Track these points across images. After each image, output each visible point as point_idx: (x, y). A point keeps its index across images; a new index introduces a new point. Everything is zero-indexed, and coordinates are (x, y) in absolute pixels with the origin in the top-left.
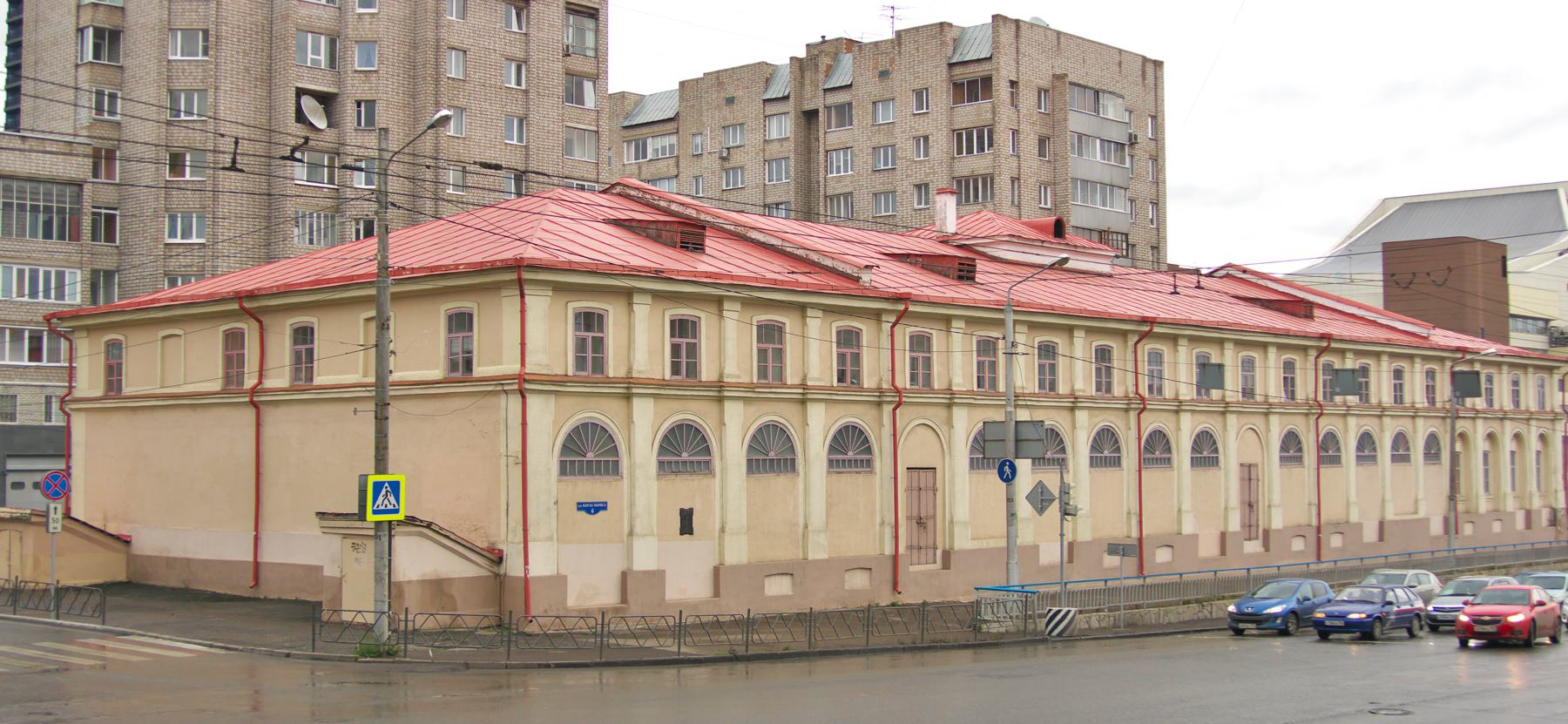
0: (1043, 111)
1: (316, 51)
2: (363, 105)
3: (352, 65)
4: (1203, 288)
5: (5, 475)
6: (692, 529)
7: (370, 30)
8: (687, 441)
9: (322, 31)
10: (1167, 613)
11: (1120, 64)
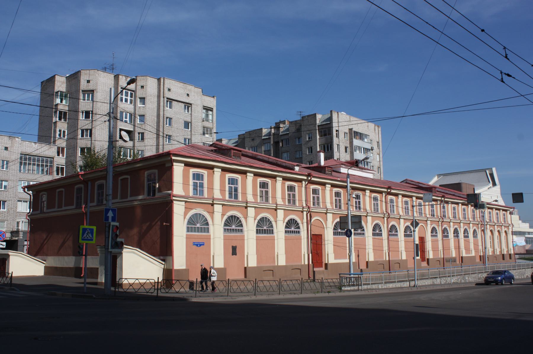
0: (346, 139)
1: (126, 118)
2: (140, 134)
3: (137, 122)
4: (504, 82)
5: (24, 247)
6: (236, 253)
7: (143, 111)
8: (234, 222)
9: (128, 112)
10: (404, 284)
11: (368, 126)
